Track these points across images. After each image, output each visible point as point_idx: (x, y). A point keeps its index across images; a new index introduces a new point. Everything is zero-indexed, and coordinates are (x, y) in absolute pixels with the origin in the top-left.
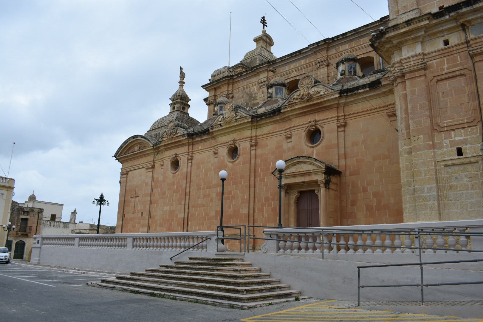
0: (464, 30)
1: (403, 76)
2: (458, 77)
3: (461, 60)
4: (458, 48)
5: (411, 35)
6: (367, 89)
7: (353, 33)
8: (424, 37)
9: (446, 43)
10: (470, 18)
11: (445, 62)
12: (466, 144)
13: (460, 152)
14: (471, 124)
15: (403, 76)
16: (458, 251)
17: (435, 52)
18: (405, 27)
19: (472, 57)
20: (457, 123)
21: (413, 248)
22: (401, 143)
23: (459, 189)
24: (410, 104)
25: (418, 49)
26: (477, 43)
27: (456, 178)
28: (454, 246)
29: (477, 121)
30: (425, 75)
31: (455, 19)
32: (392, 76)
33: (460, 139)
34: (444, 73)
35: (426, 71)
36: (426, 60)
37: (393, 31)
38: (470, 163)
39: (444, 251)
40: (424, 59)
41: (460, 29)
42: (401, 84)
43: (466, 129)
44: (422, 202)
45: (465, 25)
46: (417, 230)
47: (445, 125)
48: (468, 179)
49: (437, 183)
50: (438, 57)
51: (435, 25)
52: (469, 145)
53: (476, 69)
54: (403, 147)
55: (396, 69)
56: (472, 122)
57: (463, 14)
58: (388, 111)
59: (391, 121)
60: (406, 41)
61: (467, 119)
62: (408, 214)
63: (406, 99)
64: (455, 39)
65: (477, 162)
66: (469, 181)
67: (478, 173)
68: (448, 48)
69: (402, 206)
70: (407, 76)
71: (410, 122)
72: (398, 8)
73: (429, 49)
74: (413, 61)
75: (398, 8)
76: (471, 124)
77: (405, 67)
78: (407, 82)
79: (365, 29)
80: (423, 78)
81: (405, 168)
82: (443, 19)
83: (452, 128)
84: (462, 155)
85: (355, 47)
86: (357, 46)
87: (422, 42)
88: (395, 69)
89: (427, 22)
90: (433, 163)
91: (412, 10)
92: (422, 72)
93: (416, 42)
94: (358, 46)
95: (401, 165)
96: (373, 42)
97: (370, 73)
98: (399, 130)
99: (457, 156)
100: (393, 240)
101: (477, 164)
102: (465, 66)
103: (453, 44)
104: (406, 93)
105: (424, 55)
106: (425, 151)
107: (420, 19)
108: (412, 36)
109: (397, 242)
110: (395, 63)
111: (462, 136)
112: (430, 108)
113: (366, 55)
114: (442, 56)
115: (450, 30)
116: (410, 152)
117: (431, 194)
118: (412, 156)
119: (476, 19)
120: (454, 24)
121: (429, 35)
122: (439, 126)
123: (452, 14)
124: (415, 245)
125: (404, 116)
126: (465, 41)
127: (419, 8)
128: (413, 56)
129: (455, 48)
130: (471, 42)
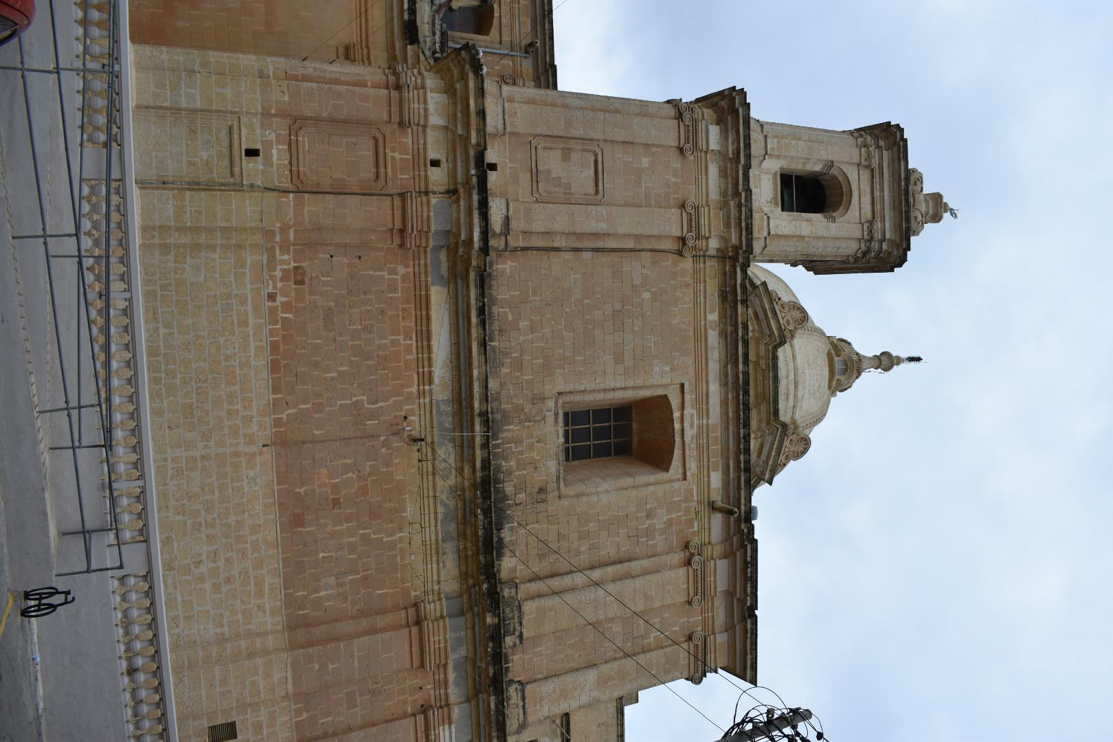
0: (448, 192)
1: (398, 87)
2: (375, 170)
3: (401, 179)
4: (423, 178)
5: (462, 113)
6: (406, 17)
7: (546, 8)
8: (454, 132)
9: (435, 163)
10: (462, 203)
11: (405, 156)
12: (264, 165)
13: (252, 153)
14: (295, 176)
15: (398, 87)
16: (82, 127)
17: (425, 144)
18: (476, 107)
19: (402, 196)
20: (301, 156)
21: (84, 57)
22: (281, 61)
23: (189, 143)
24: (346, 89)
25: (436, 120)
26: (422, 205)
27: (209, 141)
28: (90, 123)
29: (299, 185)
30: (390, 122)
31: (467, 182)
32: (403, 69)
33: (272, 156)
34: (387, 151)
35: (396, 125)
36: (415, 128)
37: (475, 87)
38: (232, 166)
39: (81, 106)
40: (418, 125)
41: (451, 187)
42: (386, 81)
43: (289, 168)
44: (170, 82)
45: (454, 195)
46: (117, 67)
47: (300, 139)
48: (205, 159)
49: (201, 111)
50: (415, 146)
51: (467, 153)
52: (261, 167)
53: (381, 197)
54: (273, 64)
55: (413, 79)
56: (299, 178)
57: (470, 195)
58: (358, 47)
59: (337, 48)
60: (455, 104)
61: (304, 171)
62: (149, 54)
63: (356, 85)
64: (437, 177)
65: (232, 176)
66: (202, 160)
67: (215, 175)
68: (425, 165)
69: (166, 44)
70: (395, 94)
71: (315, 85)
72: (518, 102)
73: (432, 136)
74: (419, 108)
75: (518, 102)
76: (295, 176)
77: (411, 94)
78: (385, 92)
79: (547, 32)
80: (385, 117)
81: (234, 62)
82: (472, 164)
83: (293, 147)
84: (246, 156)
85: (519, 4)
86: (519, 8)
87: (446, 128)
88: (414, 75)
89: (474, 141)
90: (237, 110)
91: (504, 124)
92: (395, 118)
93: (449, 118)
94: (519, 10)
95: (241, 56)
96: (470, 50)
97: (444, 25)
98: (304, 62)
99: (246, 147)
100: (99, 24)
101: (229, 175)
102: (390, 183)
103: (429, 173)
104: (366, 86)
105: (425, 127)
106: (260, 99)
107: (482, 131)
108: (459, 115)
109: (95, 31)
110: (423, 78)
111: (278, 160)
112: (333, 121)
113: (496, 21)
114: (416, 153)
115: (453, 173)
116: (262, 75)
117: (183, 99)
118: (254, 77)
119: (459, 212)
120: (460, 179)
121: (455, 140)
122: (301, 128)
123: (475, 180)
124: (91, 61)
125: (328, 76)
126: (430, 190)
127: (504, 134)
128: (426, 110)
129: (422, 173)
130: (424, 198)
